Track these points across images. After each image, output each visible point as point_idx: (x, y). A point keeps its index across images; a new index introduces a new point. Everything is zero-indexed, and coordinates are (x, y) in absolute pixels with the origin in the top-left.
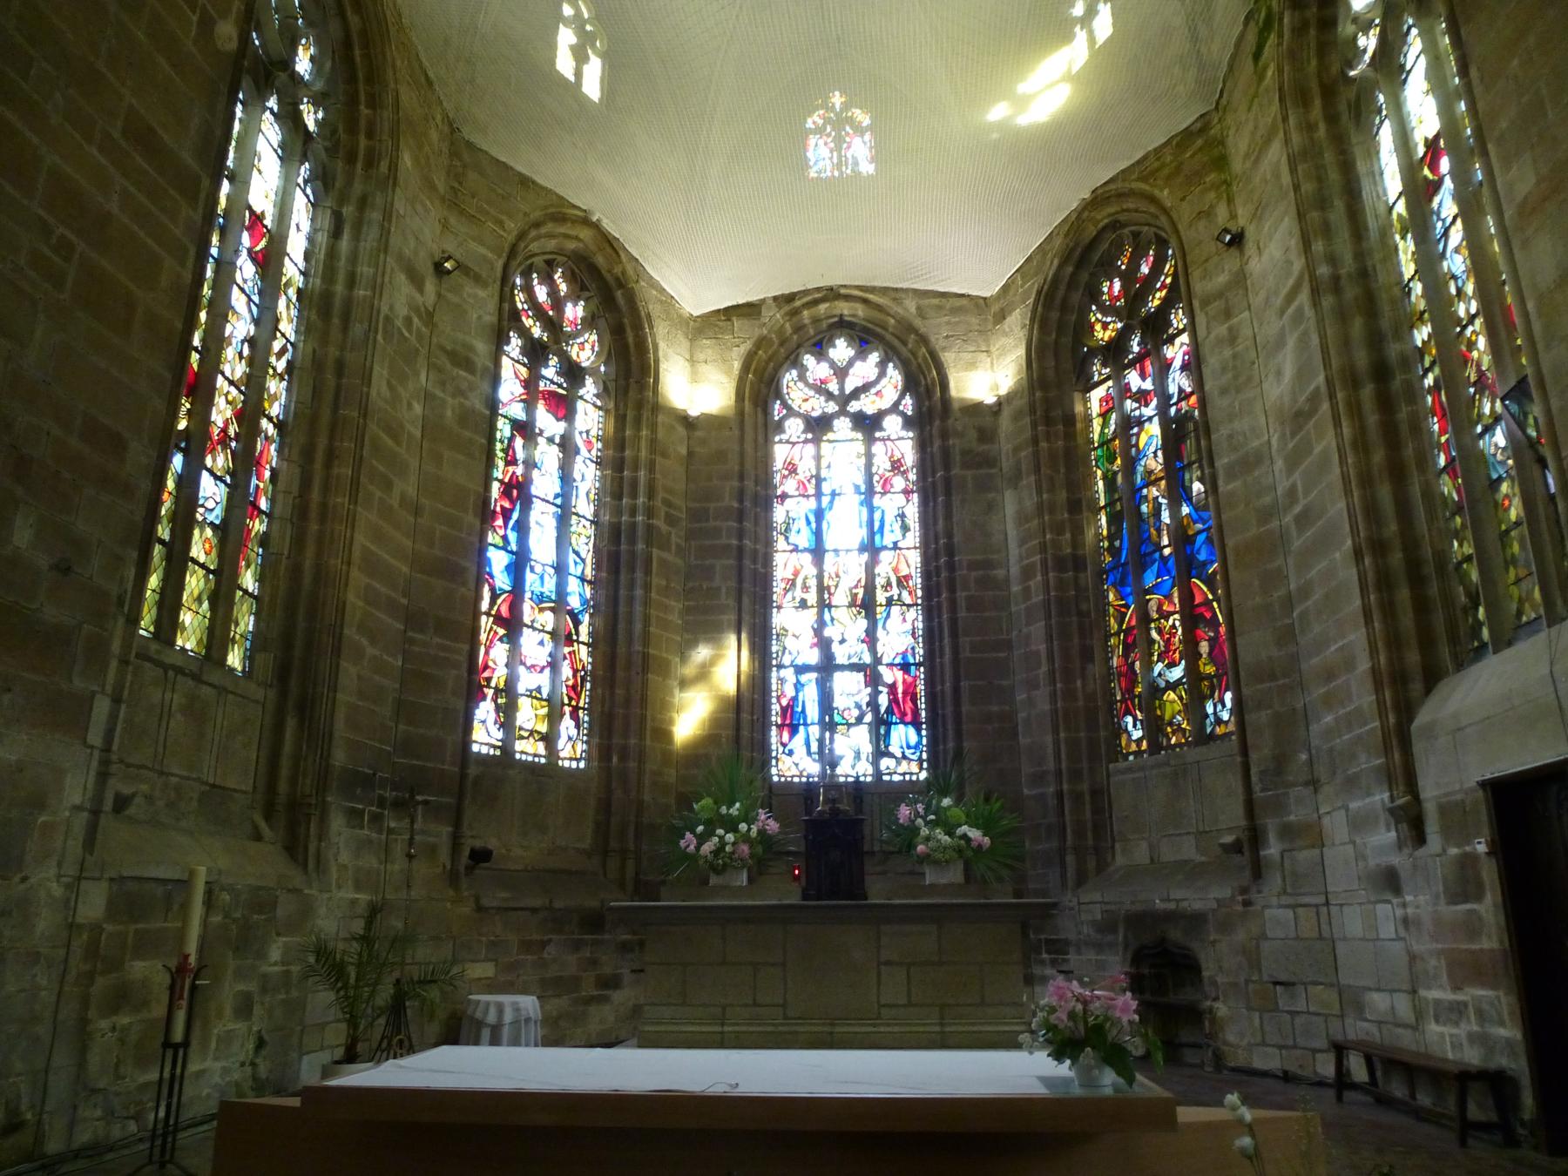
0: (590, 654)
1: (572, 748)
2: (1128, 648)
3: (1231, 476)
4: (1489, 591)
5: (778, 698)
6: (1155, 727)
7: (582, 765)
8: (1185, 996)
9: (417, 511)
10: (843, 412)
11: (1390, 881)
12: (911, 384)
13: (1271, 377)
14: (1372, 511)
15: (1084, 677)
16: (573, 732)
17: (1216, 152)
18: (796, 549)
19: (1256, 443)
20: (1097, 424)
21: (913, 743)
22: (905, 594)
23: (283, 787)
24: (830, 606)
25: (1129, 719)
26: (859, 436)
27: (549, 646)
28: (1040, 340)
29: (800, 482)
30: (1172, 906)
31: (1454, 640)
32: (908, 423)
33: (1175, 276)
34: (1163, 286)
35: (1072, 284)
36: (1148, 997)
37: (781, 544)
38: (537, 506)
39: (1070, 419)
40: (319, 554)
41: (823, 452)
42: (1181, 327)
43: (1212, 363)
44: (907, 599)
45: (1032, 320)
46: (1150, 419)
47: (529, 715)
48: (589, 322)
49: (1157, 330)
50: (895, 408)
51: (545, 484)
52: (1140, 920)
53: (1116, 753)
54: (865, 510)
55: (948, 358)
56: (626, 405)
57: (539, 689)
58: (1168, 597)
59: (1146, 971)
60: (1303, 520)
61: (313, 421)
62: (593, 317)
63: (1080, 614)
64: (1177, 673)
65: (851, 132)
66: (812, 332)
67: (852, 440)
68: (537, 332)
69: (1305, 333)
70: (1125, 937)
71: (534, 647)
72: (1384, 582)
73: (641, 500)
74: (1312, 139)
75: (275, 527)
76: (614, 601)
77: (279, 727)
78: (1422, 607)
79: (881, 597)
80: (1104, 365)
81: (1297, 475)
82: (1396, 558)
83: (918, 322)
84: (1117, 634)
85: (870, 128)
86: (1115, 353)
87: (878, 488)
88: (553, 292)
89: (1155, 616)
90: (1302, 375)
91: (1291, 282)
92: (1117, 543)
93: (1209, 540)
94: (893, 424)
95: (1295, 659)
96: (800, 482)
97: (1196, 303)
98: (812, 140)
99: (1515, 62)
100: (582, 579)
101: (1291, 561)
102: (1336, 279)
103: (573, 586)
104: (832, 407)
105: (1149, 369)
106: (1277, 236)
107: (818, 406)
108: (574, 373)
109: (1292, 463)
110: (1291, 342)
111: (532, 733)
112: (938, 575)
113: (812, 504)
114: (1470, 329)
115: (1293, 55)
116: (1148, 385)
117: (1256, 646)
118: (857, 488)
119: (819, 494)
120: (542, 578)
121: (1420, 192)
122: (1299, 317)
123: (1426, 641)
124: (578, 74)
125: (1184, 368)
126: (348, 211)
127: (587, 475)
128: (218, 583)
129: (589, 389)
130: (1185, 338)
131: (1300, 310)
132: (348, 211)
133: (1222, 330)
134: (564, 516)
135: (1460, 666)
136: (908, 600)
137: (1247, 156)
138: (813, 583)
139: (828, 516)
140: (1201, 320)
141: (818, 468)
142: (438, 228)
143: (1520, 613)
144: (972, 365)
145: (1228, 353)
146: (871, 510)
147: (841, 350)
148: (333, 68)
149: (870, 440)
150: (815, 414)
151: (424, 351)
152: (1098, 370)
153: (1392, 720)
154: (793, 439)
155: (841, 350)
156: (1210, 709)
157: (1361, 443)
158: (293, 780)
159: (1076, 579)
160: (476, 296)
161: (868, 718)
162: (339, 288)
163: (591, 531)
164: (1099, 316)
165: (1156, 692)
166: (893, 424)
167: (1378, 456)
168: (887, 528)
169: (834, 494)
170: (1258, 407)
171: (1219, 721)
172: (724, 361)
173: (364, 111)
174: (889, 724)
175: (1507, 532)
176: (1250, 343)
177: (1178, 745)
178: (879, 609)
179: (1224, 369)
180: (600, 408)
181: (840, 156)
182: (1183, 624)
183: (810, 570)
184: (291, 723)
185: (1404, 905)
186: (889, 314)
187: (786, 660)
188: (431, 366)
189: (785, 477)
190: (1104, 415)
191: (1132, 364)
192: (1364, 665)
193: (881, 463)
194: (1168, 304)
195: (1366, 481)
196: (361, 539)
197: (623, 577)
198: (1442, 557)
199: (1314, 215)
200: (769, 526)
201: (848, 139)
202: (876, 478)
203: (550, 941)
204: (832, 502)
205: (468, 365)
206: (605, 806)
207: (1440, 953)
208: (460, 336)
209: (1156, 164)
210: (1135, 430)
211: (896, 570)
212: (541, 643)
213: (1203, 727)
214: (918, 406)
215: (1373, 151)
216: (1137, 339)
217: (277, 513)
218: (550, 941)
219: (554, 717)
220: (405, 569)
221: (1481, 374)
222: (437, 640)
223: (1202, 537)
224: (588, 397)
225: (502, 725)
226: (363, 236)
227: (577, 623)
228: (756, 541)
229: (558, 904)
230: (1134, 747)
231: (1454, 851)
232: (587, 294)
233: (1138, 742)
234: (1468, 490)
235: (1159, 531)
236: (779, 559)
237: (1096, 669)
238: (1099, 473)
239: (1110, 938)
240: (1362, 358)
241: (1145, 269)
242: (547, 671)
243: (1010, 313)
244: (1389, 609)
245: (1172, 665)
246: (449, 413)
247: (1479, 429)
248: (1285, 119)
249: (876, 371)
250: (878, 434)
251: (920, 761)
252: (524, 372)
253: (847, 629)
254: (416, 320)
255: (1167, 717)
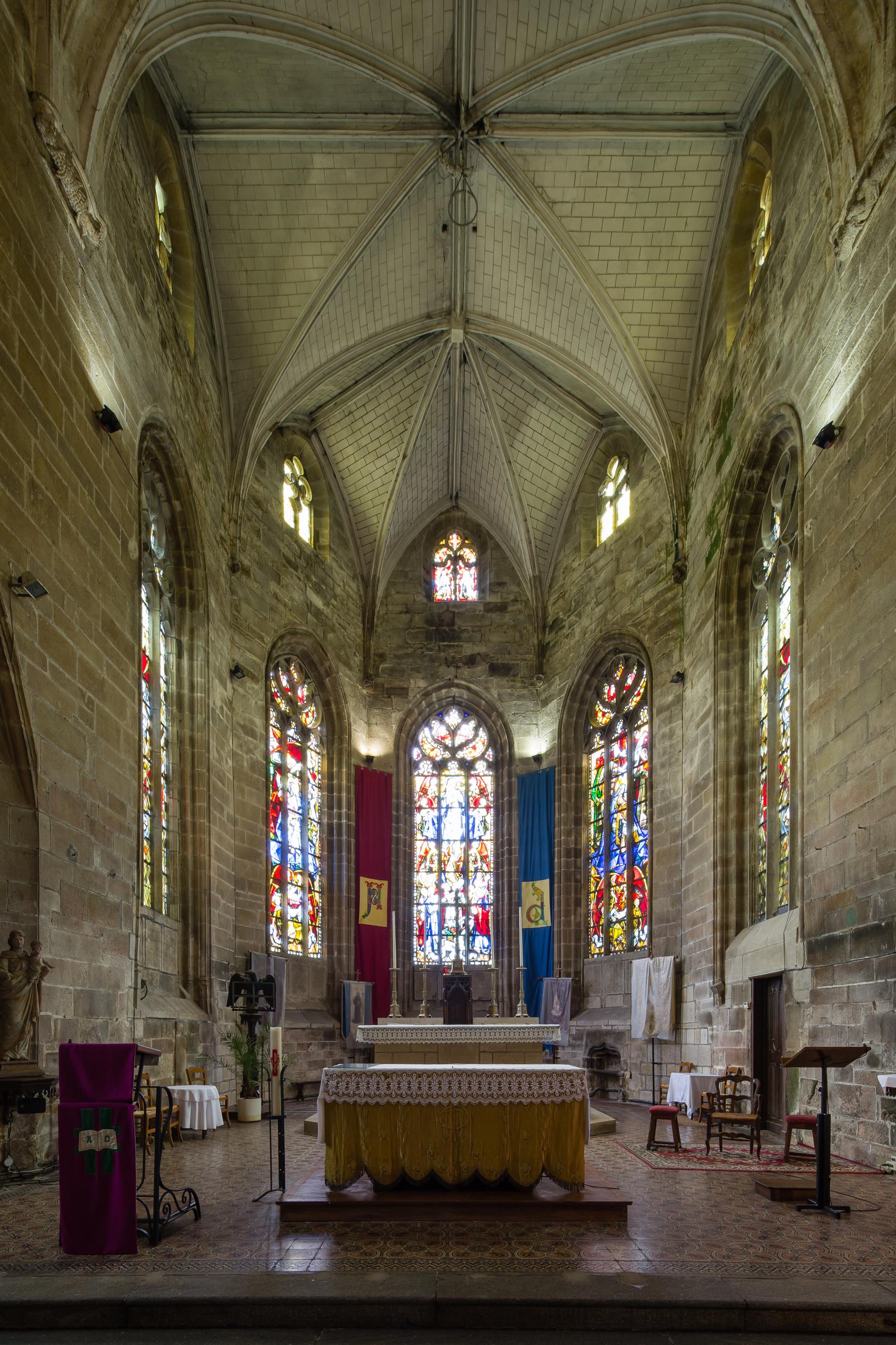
0: (321, 898)
1: (315, 948)
2: (599, 900)
3: (661, 814)
4: (770, 891)
5: (418, 922)
6: (608, 941)
7: (319, 956)
8: (612, 1069)
9: (235, 823)
10: (453, 757)
11: (708, 1019)
12: (493, 742)
13: (688, 761)
14: (725, 845)
15: (575, 914)
16: (314, 939)
17: (677, 616)
18: (427, 839)
19: (675, 798)
20: (594, 773)
21: (486, 946)
22: (485, 866)
23: (191, 972)
24: (444, 872)
25: (596, 937)
26: (462, 773)
27: (300, 894)
28: (567, 720)
29: (429, 799)
30: (610, 1028)
31: (752, 910)
32: (490, 766)
33: (646, 688)
34: (639, 694)
35: (588, 686)
36: (595, 1069)
37: (419, 836)
38: (291, 815)
39: (579, 770)
40: (194, 852)
41: (442, 782)
42: (645, 721)
43: (659, 747)
44: (485, 868)
45: (564, 707)
46: (622, 774)
47: (293, 931)
48: (311, 698)
49: (631, 719)
50: (482, 757)
51: (293, 802)
52: (593, 1035)
53: (587, 952)
54: (464, 818)
55: (514, 727)
56: (333, 752)
57: (297, 917)
58: (621, 874)
59: (595, 1058)
60: (693, 842)
61: (182, 774)
62: (313, 695)
63: (576, 881)
64: (622, 914)
65: (463, 566)
66: (437, 706)
67: (458, 776)
68: (283, 707)
69: (707, 742)
70: (586, 1042)
71: (294, 895)
72: (726, 880)
73: (344, 810)
74: (728, 624)
75: (171, 835)
76: (330, 868)
77: (185, 942)
78: (741, 893)
79: (472, 867)
80: (601, 739)
81: (692, 819)
82: (733, 868)
83: (498, 704)
84: (594, 892)
85: (475, 564)
86: (607, 731)
87: (472, 805)
88: (290, 680)
89: (614, 884)
90: (703, 764)
91: (705, 710)
92: (598, 844)
93: (645, 846)
94: (481, 766)
95: (679, 912)
96: (429, 799)
97: (655, 711)
98: (439, 571)
99: (823, 627)
100: (314, 856)
101: (684, 863)
102: (727, 713)
103: (310, 859)
104: (447, 755)
105: (626, 744)
106: (702, 680)
107: (439, 754)
108: (304, 732)
109: (692, 811)
110: (700, 745)
111: (295, 940)
112: (503, 856)
113: (435, 813)
114: (785, 754)
115: (726, 566)
116: (623, 754)
117: (661, 905)
118: (460, 804)
119: (439, 808)
120: (295, 856)
121: (776, 670)
122: (705, 732)
123: (740, 910)
124: (296, 521)
125: (644, 746)
126: (185, 639)
127: (315, 795)
128: (152, 870)
129: (313, 742)
130: (646, 728)
131: (707, 727)
132: (185, 639)
133: (666, 730)
134: (304, 820)
135: (753, 923)
136: (486, 869)
137: (694, 623)
138: (436, 858)
139: (444, 820)
140: (656, 721)
141: (439, 792)
142: (229, 644)
143: (781, 901)
144: (527, 733)
145: (667, 743)
146: (468, 818)
147: (453, 717)
148: (167, 539)
149: (468, 776)
150: (438, 759)
151: (230, 727)
152: (598, 741)
153: (719, 947)
154: (426, 774)
155: (453, 717)
156: (636, 934)
157: (726, 808)
158: (195, 969)
159: (575, 862)
160: (253, 689)
161: (464, 932)
162: (186, 691)
163: (317, 828)
164: (601, 707)
165: (610, 923)
166: (481, 766)
167: (733, 815)
168: (476, 828)
169: (448, 808)
170: (679, 777)
171: (640, 940)
172: (387, 725)
173: (186, 569)
174: (474, 936)
175: (783, 861)
176: (680, 739)
177: (620, 951)
178: (470, 874)
179: (664, 753)
180: (319, 754)
181: (456, 585)
182: (628, 890)
183: (434, 851)
184: (191, 940)
185: (713, 1030)
186: (482, 698)
187: (422, 901)
188: (235, 735)
189: (420, 796)
190: (598, 769)
191: (616, 740)
192: (710, 919)
193: (474, 790)
194: (639, 706)
195: (725, 828)
196: (214, 842)
197: (335, 854)
198: (754, 869)
199: (722, 673)
200: (412, 826)
201: (460, 572)
202: (471, 799)
203: (311, 1044)
204: (446, 812)
205: (252, 733)
206: (332, 976)
207: (723, 1050)
208: (247, 715)
209: (644, 617)
210: (614, 780)
211: (480, 852)
212: (297, 892)
213: (632, 942)
214: (496, 757)
215: (758, 637)
216: (621, 725)
217: (171, 828)
218: (311, 1044)
219: (304, 932)
220: (232, 856)
221: (786, 780)
222: (250, 893)
223: (642, 844)
224: (312, 747)
225: (280, 936)
226: (195, 657)
227: (313, 880)
228: (405, 835)
229: (314, 1026)
230: (597, 951)
231: (735, 1007)
232: (308, 681)
233: (600, 948)
234: (769, 836)
235: (620, 838)
236: (418, 844)
237: (582, 910)
238: (592, 803)
239: (579, 1042)
240: (733, 760)
241: (630, 681)
242: (300, 907)
243: (551, 701)
244: (725, 894)
245: (620, 910)
246: (245, 764)
247: (780, 807)
248: (716, 609)
249: (473, 732)
250: (472, 773)
251: (490, 955)
252: (278, 732)
253: (454, 882)
254: (225, 708)
255: (615, 937)
